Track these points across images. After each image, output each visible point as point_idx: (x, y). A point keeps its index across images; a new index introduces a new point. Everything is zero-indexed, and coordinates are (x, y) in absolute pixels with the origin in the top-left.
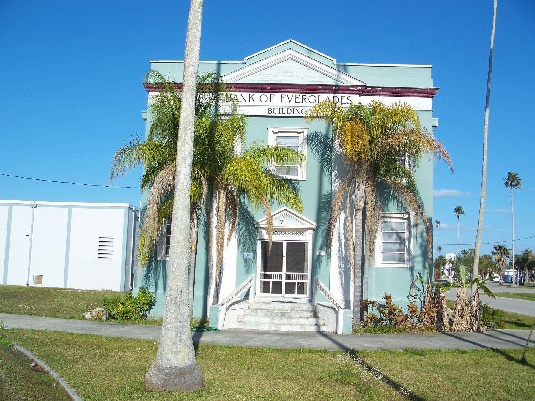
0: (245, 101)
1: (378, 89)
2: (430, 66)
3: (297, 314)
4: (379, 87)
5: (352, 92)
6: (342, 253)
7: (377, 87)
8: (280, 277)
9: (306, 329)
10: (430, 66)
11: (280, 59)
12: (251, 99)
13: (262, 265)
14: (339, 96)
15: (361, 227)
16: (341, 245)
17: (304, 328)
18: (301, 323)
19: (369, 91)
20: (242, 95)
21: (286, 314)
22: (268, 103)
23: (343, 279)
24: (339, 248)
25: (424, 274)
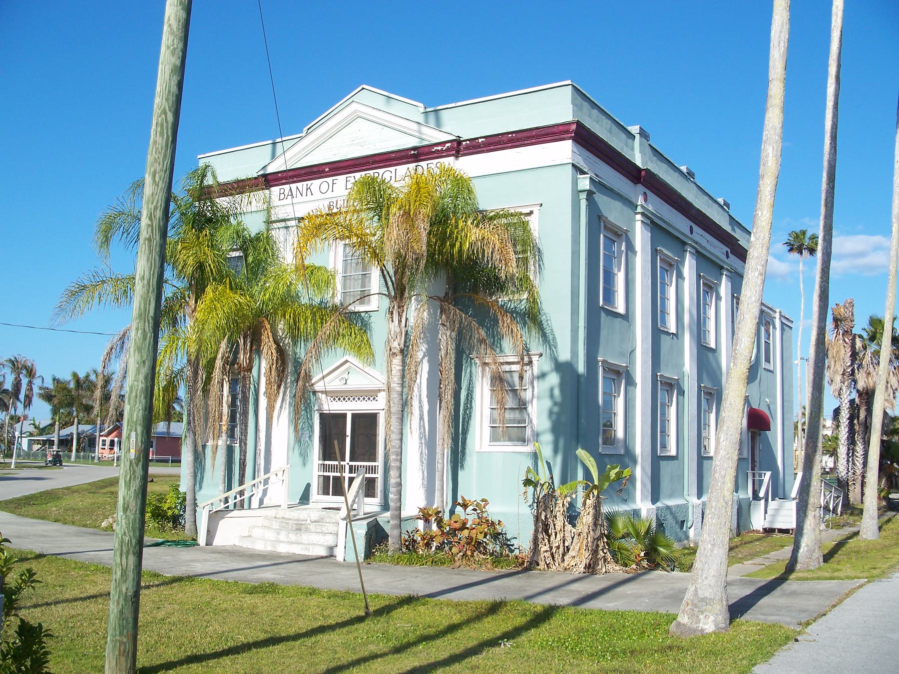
0: (302, 195)
1: (480, 140)
2: (569, 82)
3: (318, 527)
4: (481, 138)
5: (439, 155)
6: (424, 429)
7: (477, 138)
8: (342, 469)
9: (311, 551)
10: (569, 82)
11: (339, 123)
12: (309, 190)
13: (321, 447)
14: (424, 164)
15: (398, 384)
16: (423, 415)
17: (309, 550)
18: (315, 542)
19: (467, 148)
20: (297, 188)
21: (303, 527)
22: (329, 194)
23: (426, 473)
24: (420, 420)
25: (555, 464)
